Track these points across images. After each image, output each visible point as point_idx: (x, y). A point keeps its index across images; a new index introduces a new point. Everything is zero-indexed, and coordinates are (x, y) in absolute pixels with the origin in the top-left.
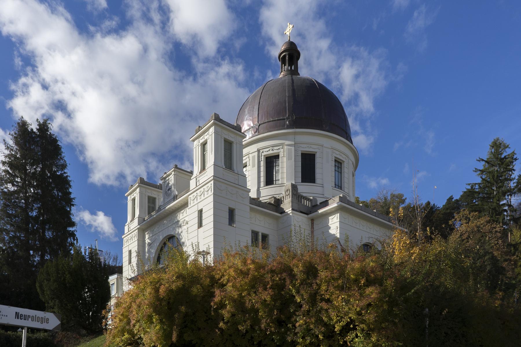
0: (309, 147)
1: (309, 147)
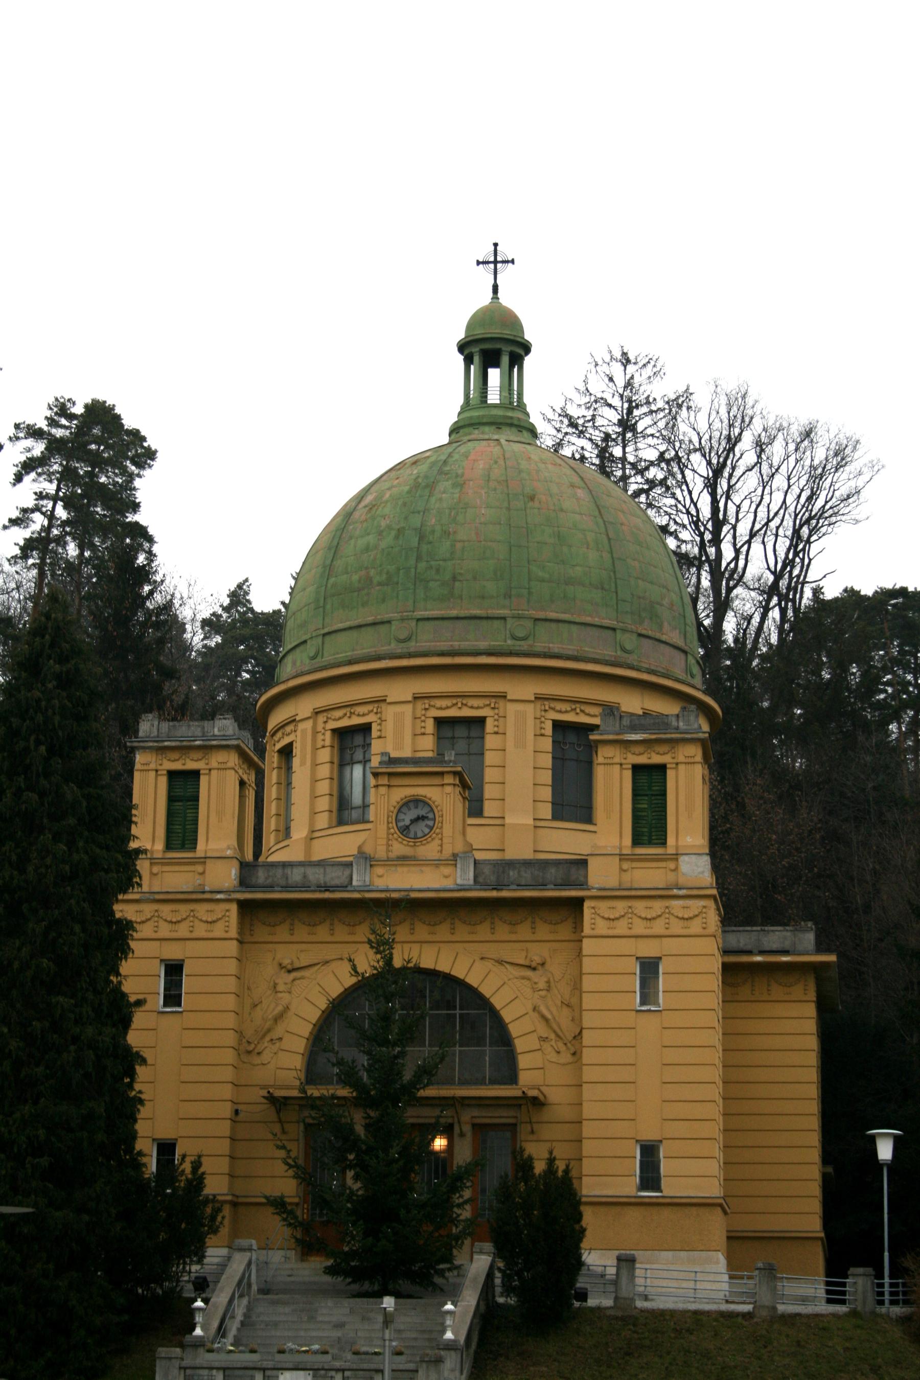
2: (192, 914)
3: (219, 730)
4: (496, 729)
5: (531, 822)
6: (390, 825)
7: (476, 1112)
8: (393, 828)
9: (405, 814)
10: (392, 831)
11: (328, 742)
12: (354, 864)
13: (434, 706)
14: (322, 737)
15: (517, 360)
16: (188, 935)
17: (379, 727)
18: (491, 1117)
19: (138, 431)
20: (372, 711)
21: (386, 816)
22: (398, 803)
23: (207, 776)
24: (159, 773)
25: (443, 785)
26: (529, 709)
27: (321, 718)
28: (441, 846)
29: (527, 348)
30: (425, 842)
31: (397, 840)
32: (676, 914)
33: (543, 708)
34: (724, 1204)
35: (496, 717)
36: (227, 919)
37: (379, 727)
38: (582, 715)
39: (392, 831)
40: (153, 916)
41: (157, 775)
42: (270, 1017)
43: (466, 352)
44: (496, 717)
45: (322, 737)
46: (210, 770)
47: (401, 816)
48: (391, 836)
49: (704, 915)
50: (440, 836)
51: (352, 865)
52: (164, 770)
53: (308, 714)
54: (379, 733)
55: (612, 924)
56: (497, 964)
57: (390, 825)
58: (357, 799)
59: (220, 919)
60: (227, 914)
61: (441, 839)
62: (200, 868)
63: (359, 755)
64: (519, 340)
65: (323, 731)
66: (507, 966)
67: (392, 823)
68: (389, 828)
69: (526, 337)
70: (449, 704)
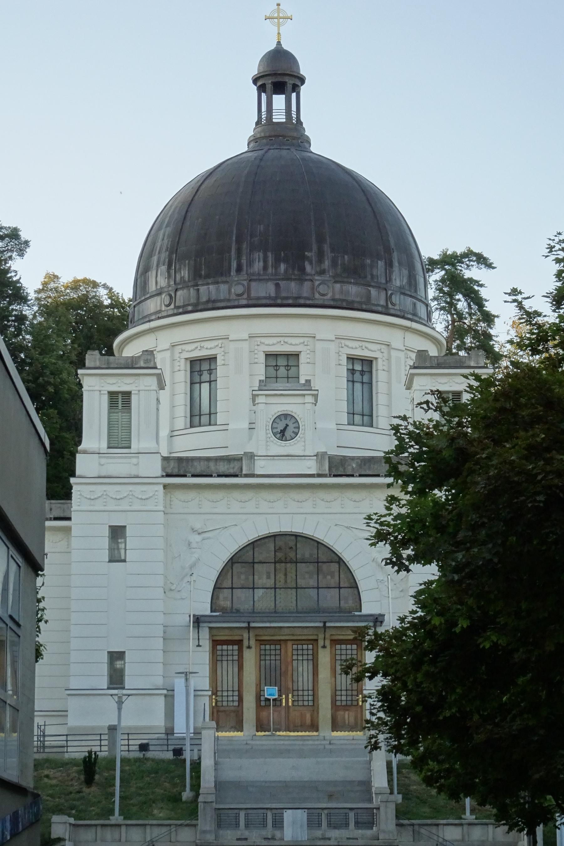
0: (282, 343)
1: (282, 343)
2: (105, 493)
3: (145, 363)
4: (308, 360)
5: (335, 427)
6: (268, 431)
7: (334, 632)
8: (270, 433)
9: (278, 424)
10: (269, 435)
11: (182, 368)
12: (243, 459)
13: (263, 343)
14: (178, 364)
15: (296, 88)
16: (128, 508)
17: (223, 358)
18: (344, 635)
19: (472, 278)
20: (217, 346)
21: (265, 425)
22: (273, 416)
23: (137, 396)
24: (102, 392)
25: (304, 403)
26: (333, 347)
27: (178, 349)
28: (305, 446)
29: (302, 80)
30: (293, 443)
31: (273, 442)
32: (85, 496)
33: (340, 346)
34: (107, 822)
35: (308, 352)
36: (156, 497)
37: (223, 358)
38: (366, 350)
39: (269, 435)
40: (128, 495)
41: (101, 394)
42: (187, 565)
43: (259, 83)
44: (308, 352)
45: (178, 364)
46: (139, 391)
47: (275, 425)
48: (268, 439)
49: (156, 497)
50: (303, 439)
51: (242, 459)
52: (106, 390)
53: (167, 346)
54: (223, 362)
55: (92, 502)
56: (345, 529)
57: (268, 431)
58: (205, 408)
59: (151, 497)
60: (156, 493)
61: (304, 442)
62: (134, 461)
63: (205, 377)
64: (296, 74)
65: (178, 359)
66: (354, 530)
67: (269, 430)
68: (267, 434)
69: (301, 73)
70: (275, 342)
